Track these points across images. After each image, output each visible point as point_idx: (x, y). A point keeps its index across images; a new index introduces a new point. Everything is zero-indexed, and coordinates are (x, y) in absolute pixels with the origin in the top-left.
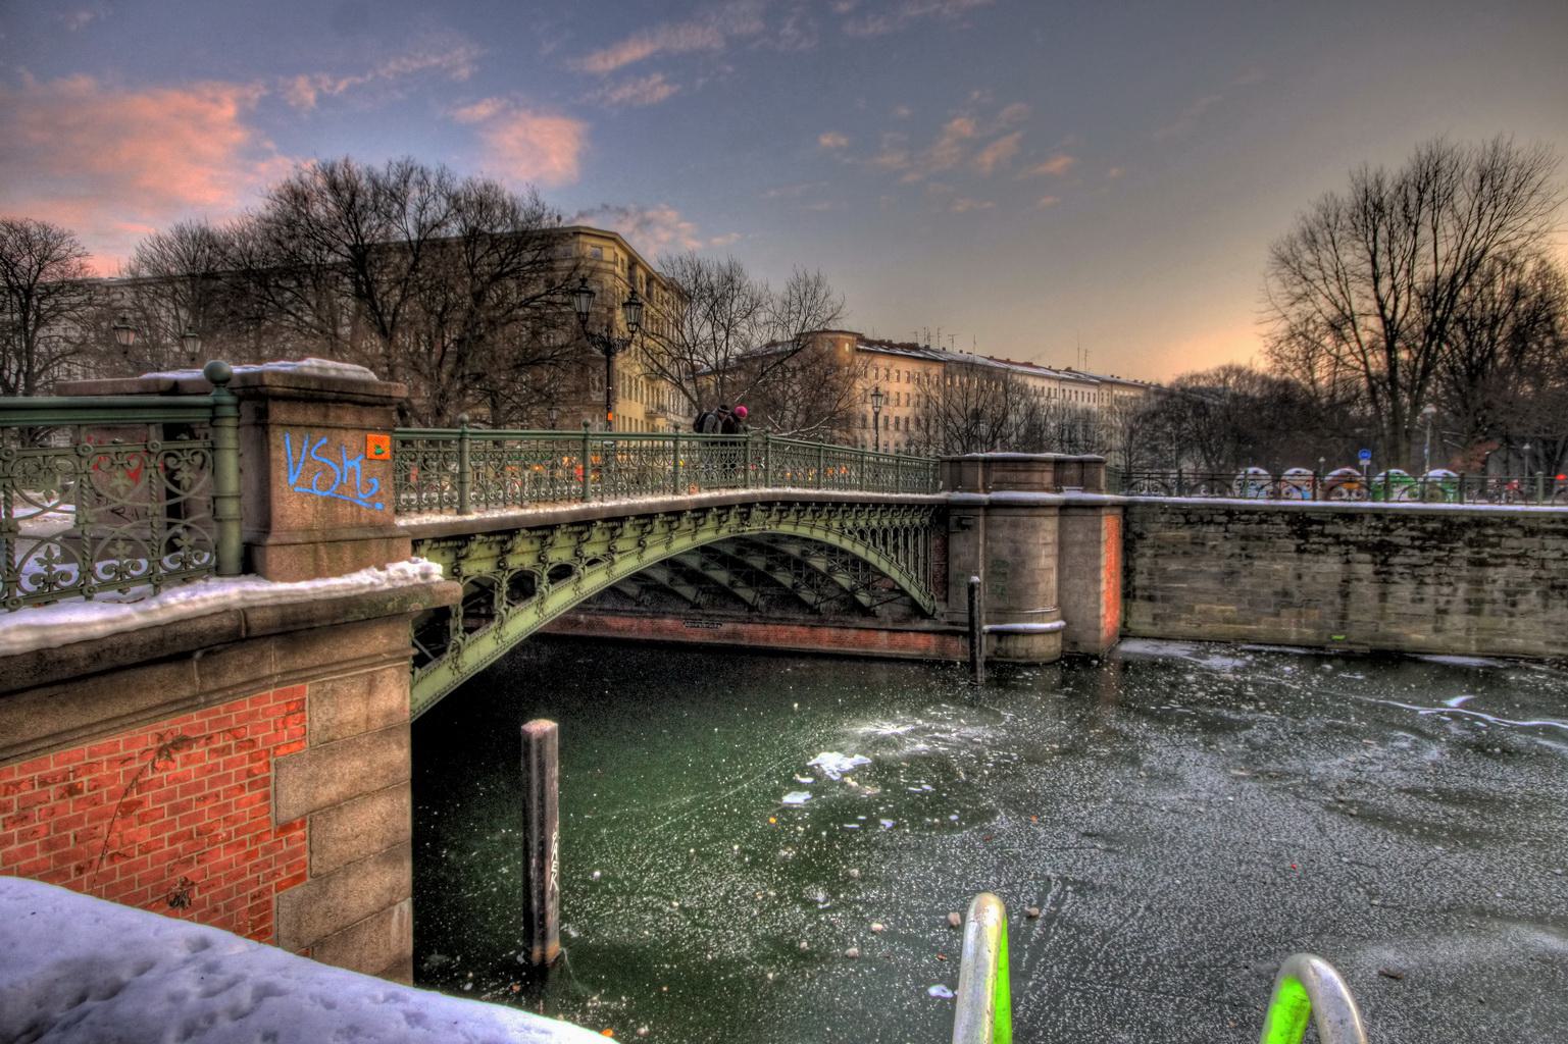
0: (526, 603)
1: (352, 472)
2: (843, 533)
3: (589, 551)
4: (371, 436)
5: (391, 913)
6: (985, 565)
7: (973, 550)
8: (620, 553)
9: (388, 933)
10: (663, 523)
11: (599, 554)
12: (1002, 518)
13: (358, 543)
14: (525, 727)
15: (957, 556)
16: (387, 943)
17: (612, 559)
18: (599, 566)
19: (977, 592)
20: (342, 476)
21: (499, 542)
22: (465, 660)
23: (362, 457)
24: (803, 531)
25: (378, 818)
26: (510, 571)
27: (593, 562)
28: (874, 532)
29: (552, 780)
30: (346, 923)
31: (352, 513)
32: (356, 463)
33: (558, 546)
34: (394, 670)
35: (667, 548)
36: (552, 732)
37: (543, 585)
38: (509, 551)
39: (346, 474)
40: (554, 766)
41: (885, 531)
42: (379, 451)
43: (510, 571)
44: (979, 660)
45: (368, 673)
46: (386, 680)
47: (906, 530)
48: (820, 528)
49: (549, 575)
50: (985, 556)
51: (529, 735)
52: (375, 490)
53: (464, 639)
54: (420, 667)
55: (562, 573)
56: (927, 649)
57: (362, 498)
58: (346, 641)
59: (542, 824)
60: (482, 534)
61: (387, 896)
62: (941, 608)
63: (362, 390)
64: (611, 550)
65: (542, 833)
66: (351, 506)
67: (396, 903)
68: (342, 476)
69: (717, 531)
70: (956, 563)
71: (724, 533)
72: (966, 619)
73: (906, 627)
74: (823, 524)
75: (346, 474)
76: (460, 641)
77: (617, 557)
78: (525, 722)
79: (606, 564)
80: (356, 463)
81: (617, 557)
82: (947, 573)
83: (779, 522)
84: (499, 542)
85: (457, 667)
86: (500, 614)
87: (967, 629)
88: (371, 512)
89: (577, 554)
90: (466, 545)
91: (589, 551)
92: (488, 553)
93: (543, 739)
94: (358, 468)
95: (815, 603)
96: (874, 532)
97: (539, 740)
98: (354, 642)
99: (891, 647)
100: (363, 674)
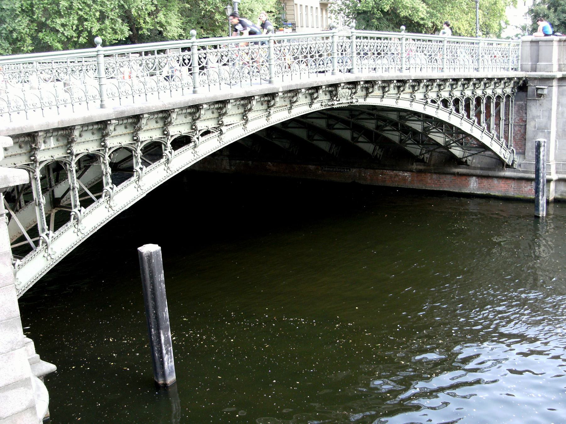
0: (157, 163)
2: (427, 102)
3: (202, 125)
6: (557, 126)
7: (546, 114)
10: (325, 93)
14: (139, 249)
15: (533, 119)
17: (221, 130)
18: (211, 135)
19: (542, 149)
21: (217, 109)
26: (142, 142)
28: (457, 101)
33: (202, 119)
35: (267, 120)
36: (156, 252)
37: (168, 150)
38: (250, 110)
40: (160, 273)
41: (478, 100)
43: (142, 142)
49: (172, 143)
50: (557, 118)
51: (141, 253)
54: (85, 208)
59: (156, 307)
60: (148, 113)
62: (518, 160)
69: (310, 105)
71: (317, 107)
72: (533, 170)
73: (491, 173)
74: (408, 96)
78: (141, 245)
79: (216, 133)
81: (224, 129)
82: (525, 132)
83: (367, 96)
84: (243, 105)
85: (111, 207)
86: (137, 171)
87: (533, 176)
89: (194, 128)
90: (296, 95)
91: (202, 125)
92: (212, 116)
93: (150, 256)
95: (421, 154)
96: (457, 101)
97: (149, 256)
99: (479, 189)
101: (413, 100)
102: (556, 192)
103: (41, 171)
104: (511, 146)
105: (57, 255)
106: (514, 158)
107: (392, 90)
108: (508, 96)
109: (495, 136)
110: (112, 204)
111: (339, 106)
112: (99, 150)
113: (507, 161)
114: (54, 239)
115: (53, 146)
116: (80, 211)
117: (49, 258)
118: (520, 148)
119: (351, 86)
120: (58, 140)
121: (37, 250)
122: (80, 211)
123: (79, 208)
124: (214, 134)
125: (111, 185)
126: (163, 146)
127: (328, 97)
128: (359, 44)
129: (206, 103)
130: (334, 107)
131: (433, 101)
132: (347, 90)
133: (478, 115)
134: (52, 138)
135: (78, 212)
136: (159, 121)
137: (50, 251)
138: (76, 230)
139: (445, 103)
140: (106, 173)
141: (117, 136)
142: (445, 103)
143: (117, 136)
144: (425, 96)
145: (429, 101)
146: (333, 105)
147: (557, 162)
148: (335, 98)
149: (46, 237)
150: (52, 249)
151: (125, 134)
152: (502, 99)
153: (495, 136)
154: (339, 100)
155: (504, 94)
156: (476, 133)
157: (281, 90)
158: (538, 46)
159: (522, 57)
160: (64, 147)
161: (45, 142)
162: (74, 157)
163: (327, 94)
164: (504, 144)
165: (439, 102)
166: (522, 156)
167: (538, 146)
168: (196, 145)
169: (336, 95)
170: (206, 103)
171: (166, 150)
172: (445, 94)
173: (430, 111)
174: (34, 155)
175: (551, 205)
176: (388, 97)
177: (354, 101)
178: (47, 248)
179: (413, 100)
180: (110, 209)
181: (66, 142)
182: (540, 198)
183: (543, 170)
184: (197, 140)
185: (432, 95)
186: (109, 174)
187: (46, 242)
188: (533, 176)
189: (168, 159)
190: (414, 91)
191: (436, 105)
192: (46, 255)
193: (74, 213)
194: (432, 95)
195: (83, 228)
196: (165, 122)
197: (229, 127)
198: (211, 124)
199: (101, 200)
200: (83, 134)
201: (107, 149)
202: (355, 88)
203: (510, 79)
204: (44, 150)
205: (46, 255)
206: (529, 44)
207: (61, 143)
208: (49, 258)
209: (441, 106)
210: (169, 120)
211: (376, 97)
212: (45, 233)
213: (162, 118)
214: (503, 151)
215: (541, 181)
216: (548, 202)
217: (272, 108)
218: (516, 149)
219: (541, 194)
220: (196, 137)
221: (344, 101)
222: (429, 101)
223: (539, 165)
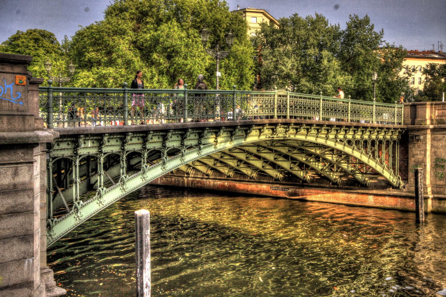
1: (9, 90)
3: (187, 143)
4: (18, 76)
5: (24, 262)
7: (423, 153)
8: (204, 145)
9: (22, 269)
11: (193, 144)
12: (441, 136)
13: (10, 117)
15: (413, 156)
16: (22, 274)
17: (200, 147)
19: (419, 175)
20: (4, 91)
22: (127, 186)
23: (13, 84)
24: (321, 141)
25: (18, 223)
27: (191, 147)
29: (146, 236)
30: (3, 261)
31: (9, 105)
32: (11, 86)
34: (26, 167)
37: (165, 157)
39: (6, 90)
40: (147, 229)
42: (21, 82)
44: (421, 212)
45: (14, 167)
46: (23, 171)
47: (381, 142)
48: (331, 140)
52: (19, 97)
53: (126, 177)
55: (173, 153)
56: (396, 205)
57: (13, 100)
58: (4, 153)
61: (23, 255)
63: (12, 58)
64: (200, 144)
65: (141, 258)
66: (9, 102)
67: (26, 258)
68: (4, 91)
70: (413, 159)
74: (324, 136)
75: (6, 90)
76: (124, 177)
77: (202, 146)
80: (11, 86)
81: (202, 146)
82: (408, 165)
83: (296, 134)
86: (143, 168)
87: (414, 195)
88: (18, 105)
89: (182, 145)
94: (11, 87)
98: (8, 154)
99: (375, 203)
100: (12, 167)
101: (327, 138)
102: (432, 207)
103: (104, 159)
104: (397, 174)
105: (83, 217)
106: (400, 183)
107: (313, 132)
108: (395, 142)
109: (386, 166)
110: (124, 187)
111: (277, 138)
112: (120, 152)
113: (395, 184)
114: (83, 206)
115: (89, 146)
116: (103, 189)
117: (78, 219)
118: (404, 176)
119: (285, 126)
120: (93, 143)
121: (70, 213)
122: (103, 189)
123: (102, 187)
124: (195, 149)
125: (125, 175)
126: (162, 154)
127: (271, 131)
128: (291, 100)
129: (131, 132)
130: (274, 139)
131: (341, 141)
132: (283, 129)
133: (373, 153)
134: (90, 141)
135: (101, 190)
136: (140, 139)
137: (79, 214)
138: (98, 202)
139: (349, 142)
140: (123, 167)
141: (153, 142)
142: (349, 142)
143: (153, 142)
144: (335, 137)
145: (338, 140)
146: (273, 137)
147: (436, 196)
148: (275, 133)
149: (77, 205)
150: (80, 213)
151: (137, 144)
152: (391, 143)
153: (386, 166)
154: (277, 135)
155: (392, 140)
156: (372, 163)
157: (239, 124)
158: (416, 108)
159: (404, 116)
160: (97, 148)
161: (85, 143)
162: (103, 155)
163: (70, 143)
164: (392, 172)
165: (345, 142)
166: (406, 181)
167: (416, 172)
168: (183, 155)
169: (276, 132)
170: (131, 132)
171: (163, 156)
172: (349, 136)
173: (339, 147)
174: (76, 151)
175: (430, 216)
176: (310, 136)
177: (287, 136)
178: (77, 212)
179: (327, 138)
180: (123, 191)
181: (73, 146)
182: (420, 208)
183: (421, 189)
184: (184, 152)
185: (341, 136)
186: (124, 168)
187: (77, 208)
188: (414, 195)
189: (164, 162)
190: (328, 132)
191: (343, 143)
192: (76, 216)
193: (98, 190)
194: (341, 136)
195: (104, 201)
196: (100, 143)
197: (205, 146)
198: (194, 143)
199: (118, 184)
200: (110, 140)
201: (78, 157)
202: (288, 128)
203: (395, 129)
204: (84, 148)
205: (76, 216)
206: (409, 107)
207: (95, 145)
208: (78, 219)
209: (347, 144)
210: (202, 135)
211: (302, 134)
212: (77, 202)
213: (121, 139)
214: (392, 177)
215: (420, 196)
216: (426, 213)
217: (233, 136)
218: (402, 177)
219: (420, 206)
220: (183, 150)
221: (280, 135)
222: (338, 140)
223: (418, 186)
